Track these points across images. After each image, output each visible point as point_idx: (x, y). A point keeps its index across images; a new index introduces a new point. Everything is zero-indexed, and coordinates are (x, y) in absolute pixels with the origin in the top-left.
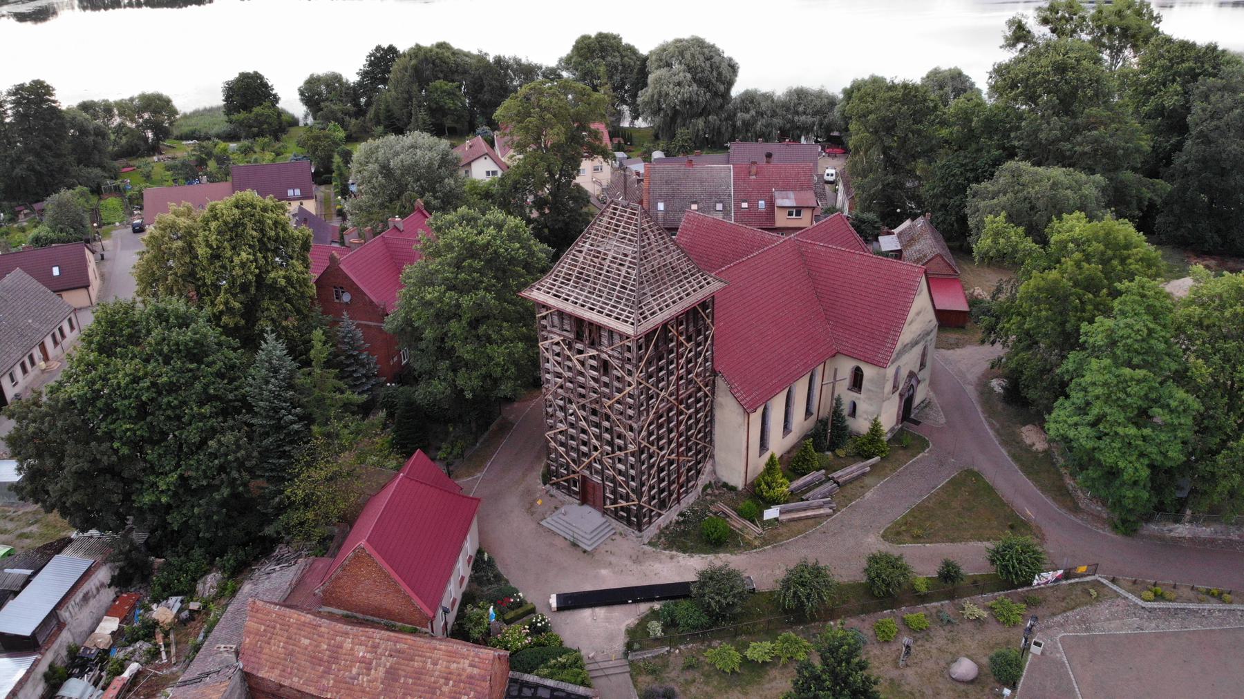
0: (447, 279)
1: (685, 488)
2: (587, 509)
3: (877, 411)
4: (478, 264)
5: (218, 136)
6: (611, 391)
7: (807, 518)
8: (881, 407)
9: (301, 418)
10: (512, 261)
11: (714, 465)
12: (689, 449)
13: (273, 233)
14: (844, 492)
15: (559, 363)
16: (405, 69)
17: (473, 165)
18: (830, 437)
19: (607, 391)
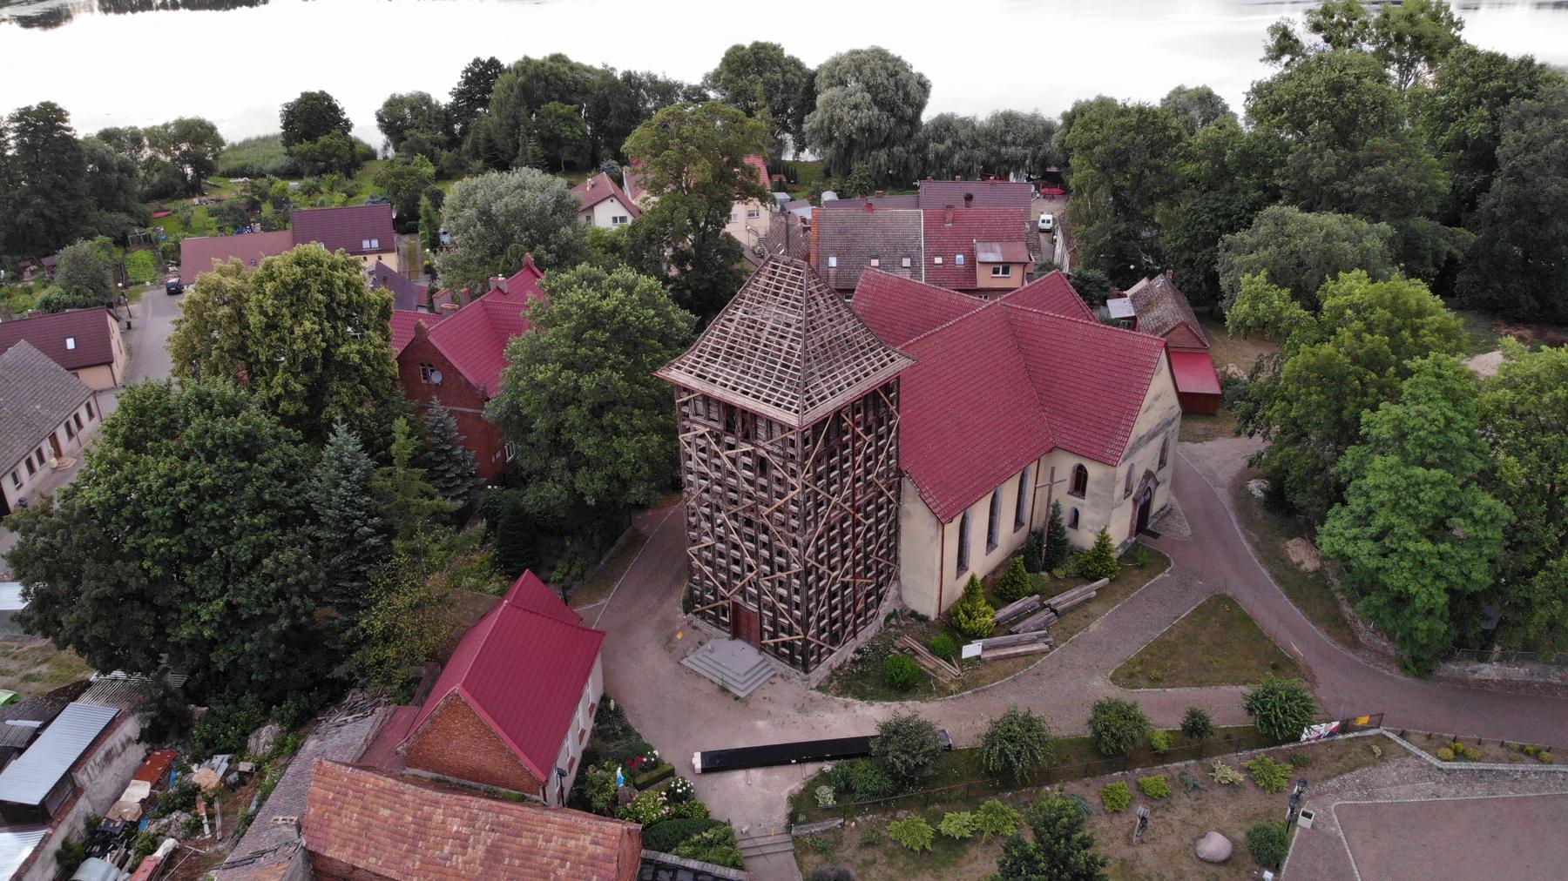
1: (863, 617)
2: (739, 644)
3: (1105, 521)
4: (602, 336)
5: (275, 173)
6: (770, 497)
7: (1017, 655)
9: (379, 531)
10: (646, 332)
11: (899, 588)
12: (868, 569)
15: (704, 461)
18: (1045, 553)
19: (765, 495)
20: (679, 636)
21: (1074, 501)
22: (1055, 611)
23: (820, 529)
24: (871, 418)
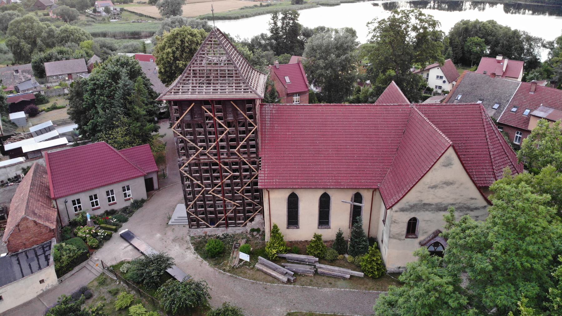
7: (270, 275)
17: (430, 70)
22: (316, 271)
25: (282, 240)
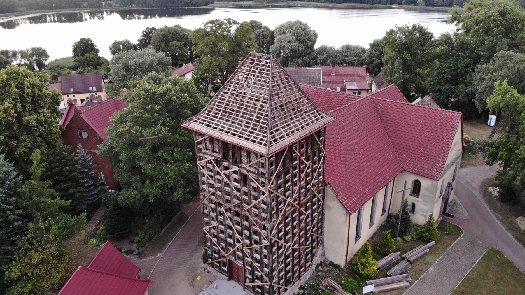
0: (136, 117)
1: (304, 267)
2: (233, 283)
3: (426, 210)
4: (157, 107)
5: (69, 68)
6: (249, 198)
7: (392, 289)
8: (433, 208)
9: (22, 217)
10: (182, 105)
11: (323, 249)
12: (307, 240)
13: (30, 91)
14: (415, 269)
15: (211, 177)
16: (159, 35)
18: (398, 225)
19: (246, 198)
20: (198, 278)
21: (411, 199)
23: (280, 219)
24: (309, 151)
25: (394, 32)
